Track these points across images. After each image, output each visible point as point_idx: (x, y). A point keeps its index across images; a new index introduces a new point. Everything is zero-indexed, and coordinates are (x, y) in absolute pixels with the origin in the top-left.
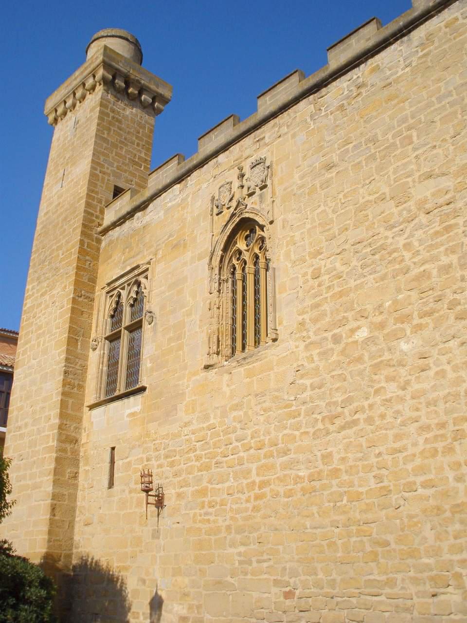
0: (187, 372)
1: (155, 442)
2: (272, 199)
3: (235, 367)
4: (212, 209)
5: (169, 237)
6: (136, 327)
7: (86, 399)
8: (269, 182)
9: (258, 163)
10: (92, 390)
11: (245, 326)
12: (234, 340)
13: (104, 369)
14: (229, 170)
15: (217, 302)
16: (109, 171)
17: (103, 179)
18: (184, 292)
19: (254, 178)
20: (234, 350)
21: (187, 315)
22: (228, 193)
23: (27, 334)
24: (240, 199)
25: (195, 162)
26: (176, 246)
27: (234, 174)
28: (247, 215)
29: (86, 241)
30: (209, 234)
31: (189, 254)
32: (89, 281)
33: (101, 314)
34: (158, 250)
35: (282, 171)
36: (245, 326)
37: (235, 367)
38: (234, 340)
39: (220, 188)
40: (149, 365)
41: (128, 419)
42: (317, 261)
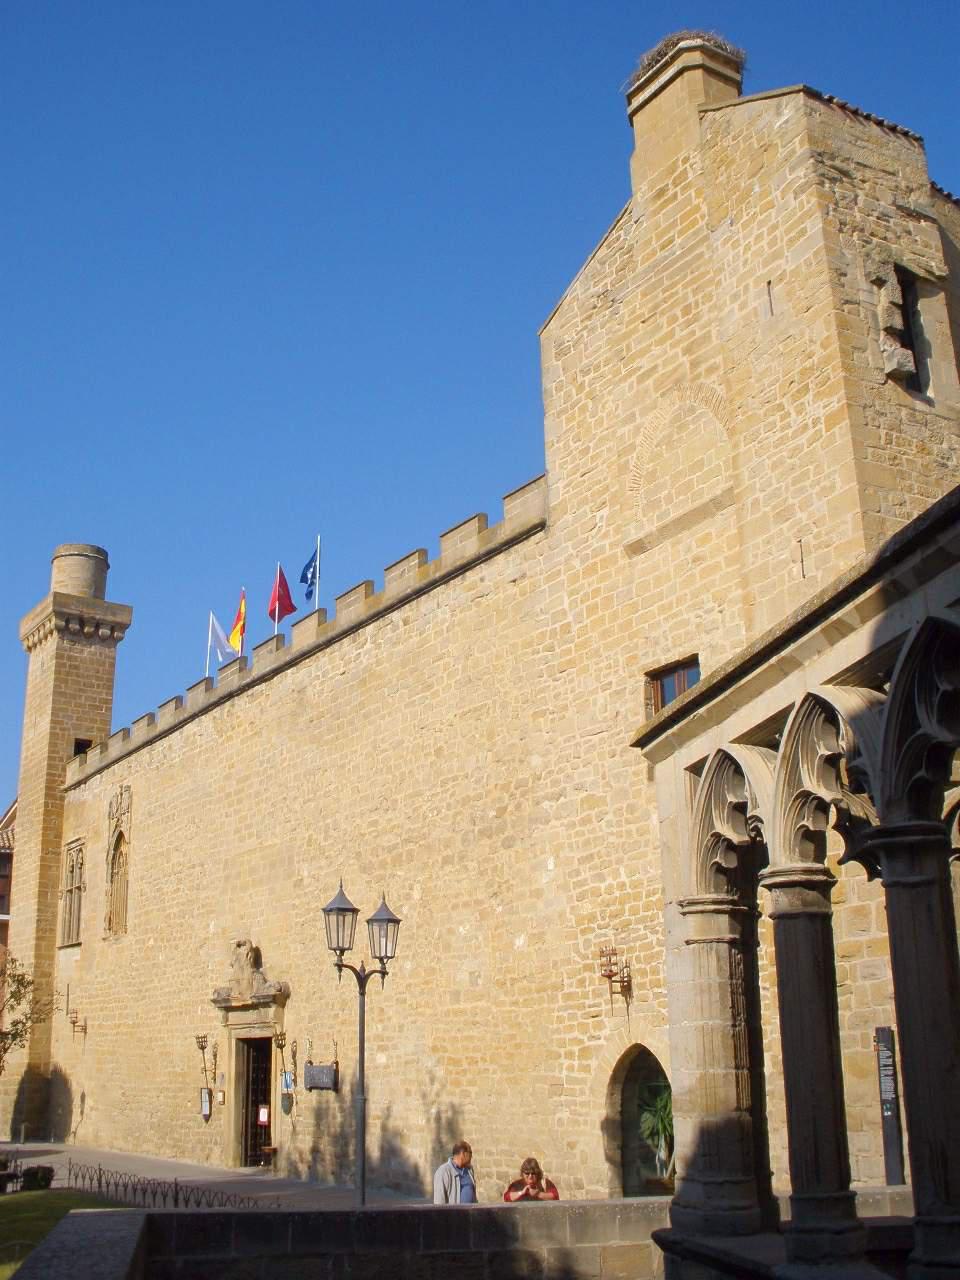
16: (69, 726)
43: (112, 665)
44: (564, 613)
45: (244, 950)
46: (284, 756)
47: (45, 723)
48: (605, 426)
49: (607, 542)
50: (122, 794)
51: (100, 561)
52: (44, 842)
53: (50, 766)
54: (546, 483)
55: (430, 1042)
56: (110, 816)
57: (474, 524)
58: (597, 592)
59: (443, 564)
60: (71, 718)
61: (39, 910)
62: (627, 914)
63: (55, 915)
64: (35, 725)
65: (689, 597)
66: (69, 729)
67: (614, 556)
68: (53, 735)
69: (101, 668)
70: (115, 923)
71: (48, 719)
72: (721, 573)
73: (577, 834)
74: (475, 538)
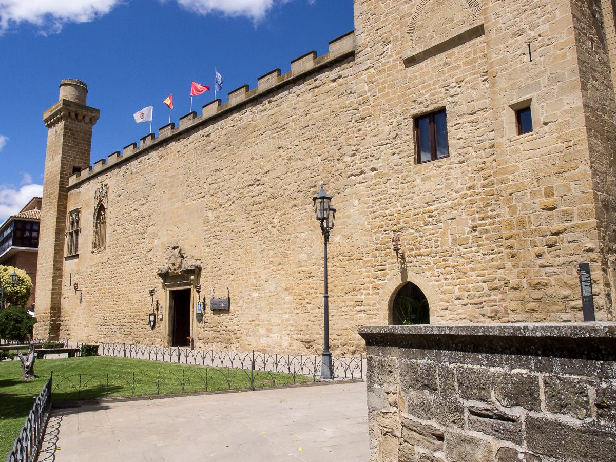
6: (77, 232)
16: (70, 160)
17: (67, 164)
29: (61, 193)
43: (91, 135)
44: (365, 93)
45: (177, 251)
46: (197, 165)
47: (58, 158)
48: (391, 6)
49: (391, 59)
50: (102, 188)
51: (82, 89)
52: (58, 211)
53: (61, 177)
54: (354, 35)
55: (284, 286)
56: (96, 198)
57: (244, 89)
58: (385, 82)
59: (292, 74)
60: (71, 156)
61: (56, 241)
62: (514, 202)
63: (63, 244)
64: (52, 160)
65: (441, 81)
66: (70, 162)
67: (396, 65)
68: (63, 163)
69: (85, 136)
70: (99, 243)
71: (60, 156)
72: (461, 69)
73: (372, 189)
74: (244, 95)
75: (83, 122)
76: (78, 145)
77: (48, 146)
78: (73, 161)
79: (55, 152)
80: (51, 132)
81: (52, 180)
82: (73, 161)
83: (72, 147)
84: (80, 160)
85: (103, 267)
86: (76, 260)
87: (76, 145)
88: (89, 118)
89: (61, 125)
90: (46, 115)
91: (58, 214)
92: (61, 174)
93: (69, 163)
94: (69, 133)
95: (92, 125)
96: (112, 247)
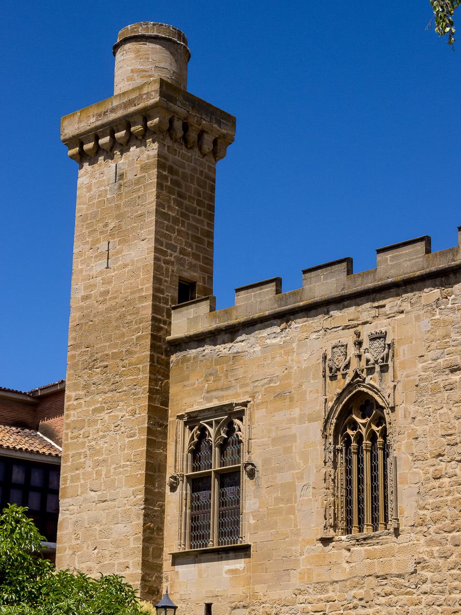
0: (300, 539)
1: (264, 605)
2: (394, 384)
3: (354, 545)
4: (324, 371)
5: (271, 381)
6: (230, 478)
7: (167, 543)
8: (390, 363)
9: (378, 335)
10: (174, 539)
11: (362, 504)
12: (349, 512)
13: (187, 512)
14: (343, 329)
15: (332, 473)
16: (172, 259)
17: (167, 270)
18: (289, 454)
19: (373, 352)
20: (349, 522)
21: (298, 478)
22: (343, 357)
23: (131, 445)
24: (358, 370)
25: (301, 304)
26: (280, 396)
27: (348, 338)
28: (363, 389)
29: (156, 355)
30: (318, 398)
31: (296, 412)
32: (161, 405)
33: (180, 446)
34: (256, 392)
35: (404, 353)
36: (362, 504)
37: (354, 545)
38: (349, 512)
39: (333, 348)
40: (252, 521)
41: (227, 576)
42: (438, 461)
43: (213, 189)
75: (197, 150)
76: (188, 217)
77: (85, 218)
78: (180, 262)
79: (121, 234)
80: (93, 181)
81: (114, 314)
82: (180, 262)
83: (176, 221)
84: (194, 262)
85: (388, 589)
86: (239, 564)
87: (183, 215)
88: (213, 138)
89: (151, 150)
90: (72, 127)
91: (149, 418)
92: (155, 298)
93: (170, 268)
94: (169, 177)
95: (216, 161)
96: (433, 528)
